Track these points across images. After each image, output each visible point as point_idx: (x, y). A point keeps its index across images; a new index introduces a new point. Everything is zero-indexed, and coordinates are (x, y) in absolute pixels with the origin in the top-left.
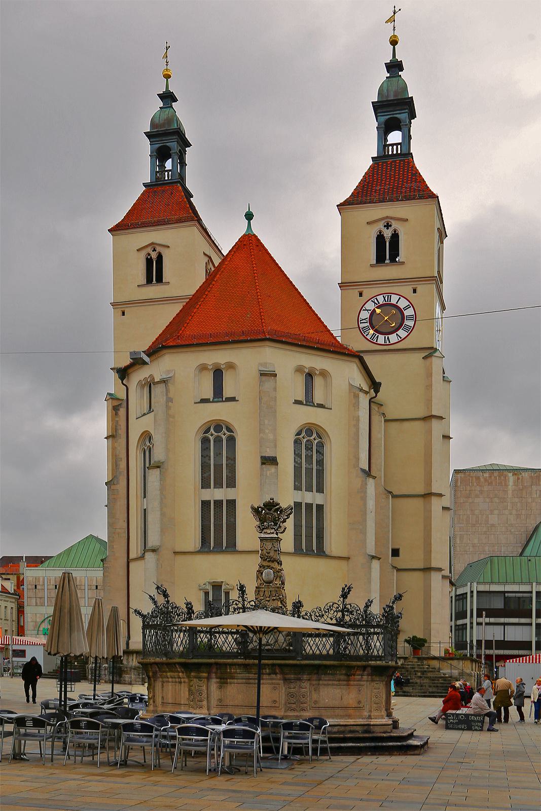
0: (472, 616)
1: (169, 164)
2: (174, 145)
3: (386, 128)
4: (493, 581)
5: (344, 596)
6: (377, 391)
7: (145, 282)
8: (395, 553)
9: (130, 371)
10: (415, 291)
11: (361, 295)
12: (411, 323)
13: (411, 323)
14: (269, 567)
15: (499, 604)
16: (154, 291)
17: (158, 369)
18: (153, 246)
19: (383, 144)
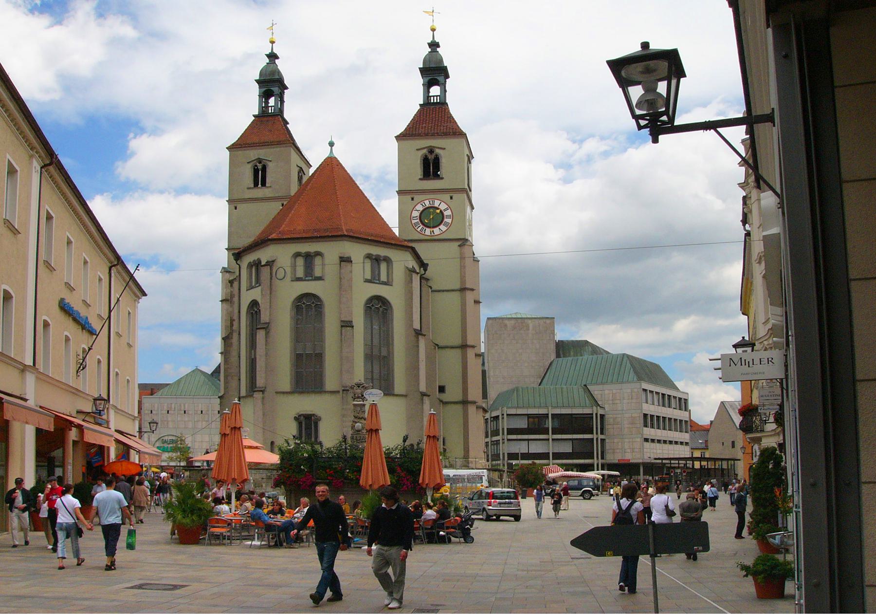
0: (503, 434)
1: (272, 101)
2: (276, 90)
3: (428, 85)
4: (519, 406)
5: (405, 441)
6: (425, 270)
7: (252, 186)
8: (442, 389)
9: (242, 254)
10: (451, 198)
11: (413, 199)
12: (449, 221)
13: (449, 221)
14: (358, 422)
15: (523, 424)
16: (260, 192)
17: (264, 255)
18: (260, 161)
19: (427, 96)
